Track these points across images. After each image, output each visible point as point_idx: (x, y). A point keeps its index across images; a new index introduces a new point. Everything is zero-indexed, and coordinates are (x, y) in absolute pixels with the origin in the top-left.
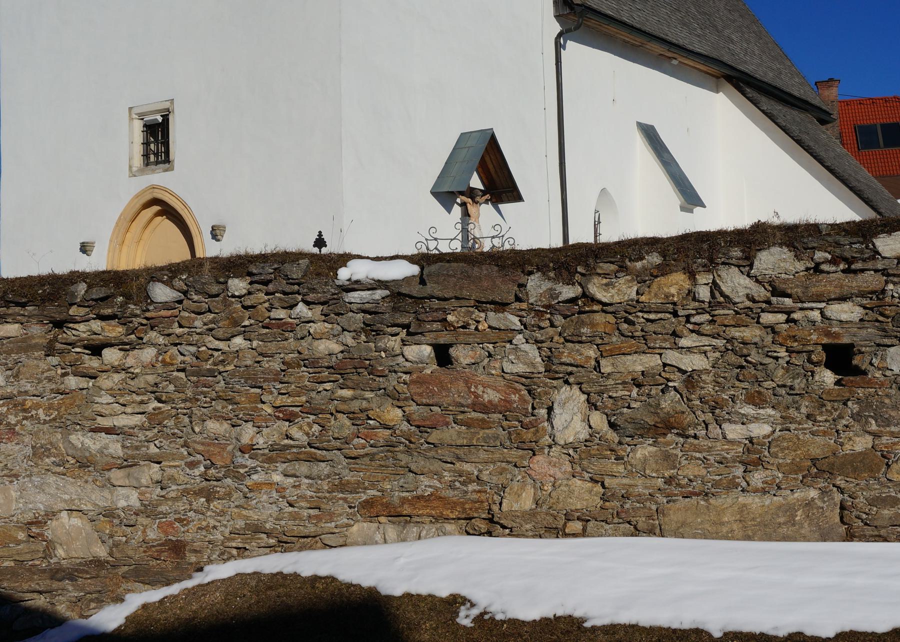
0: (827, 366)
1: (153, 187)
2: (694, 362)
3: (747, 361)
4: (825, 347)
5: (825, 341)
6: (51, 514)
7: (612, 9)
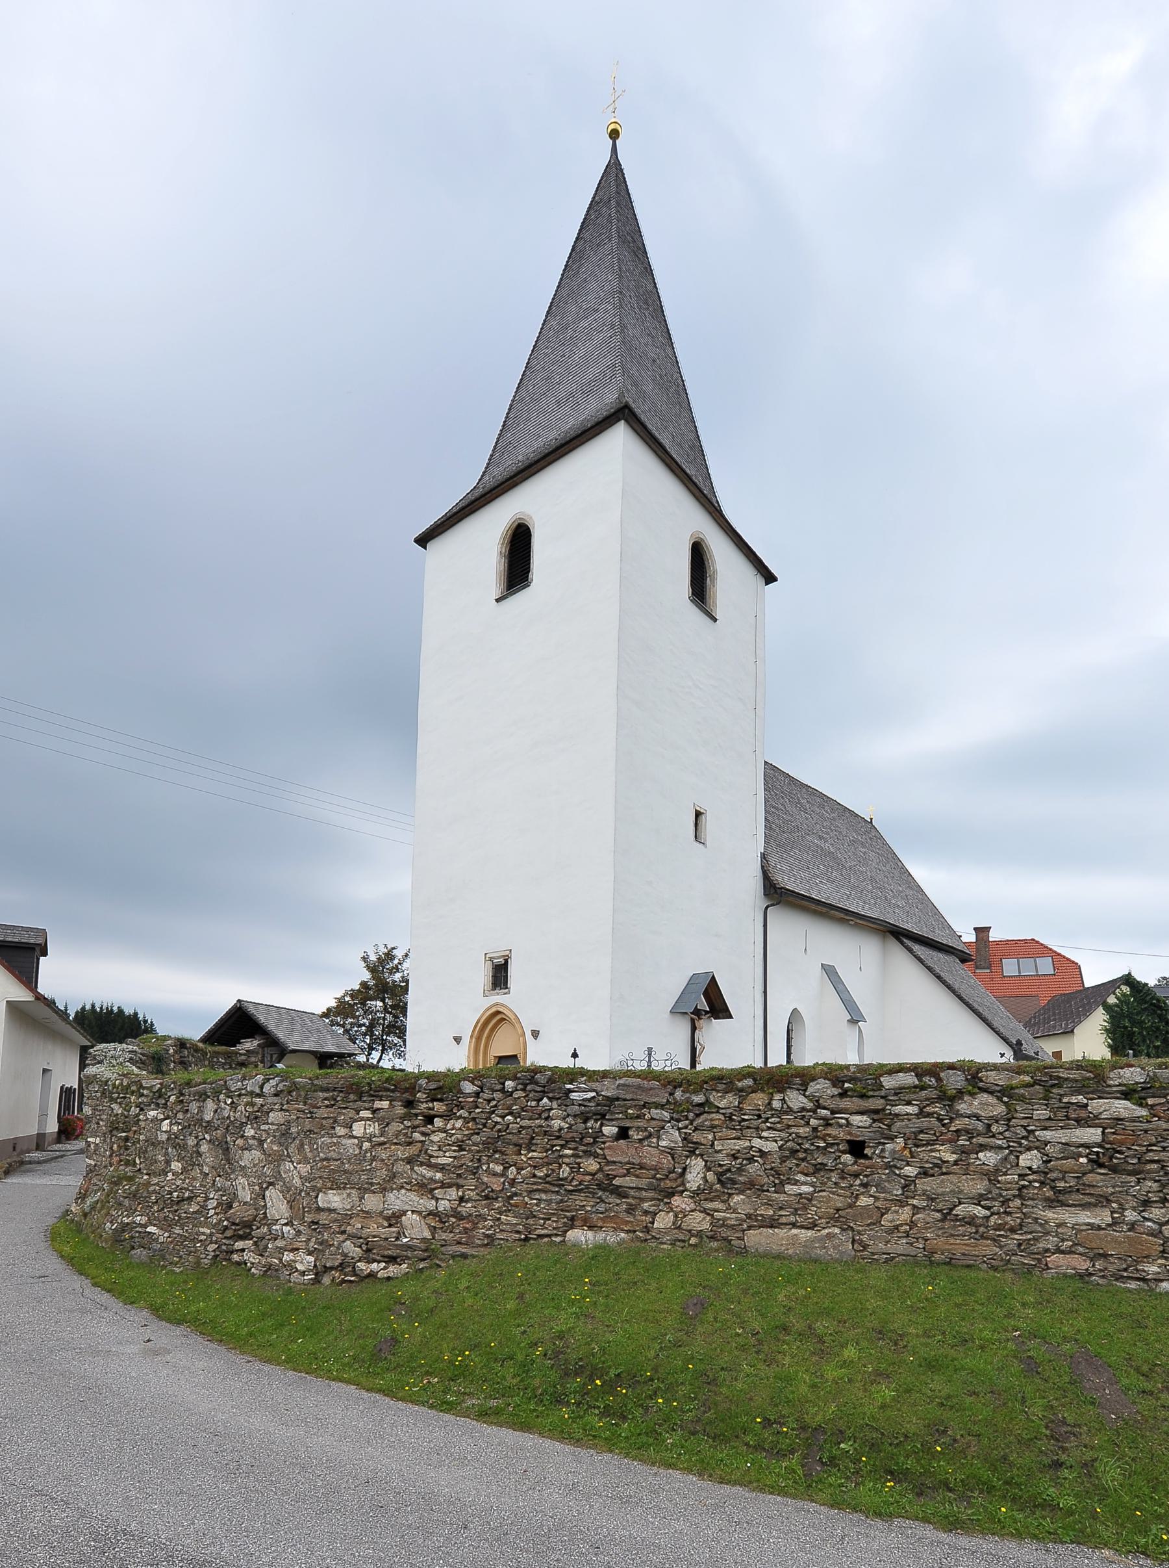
0: (850, 1153)
1: (497, 1004)
2: (769, 1146)
3: (801, 1148)
4: (848, 1142)
5: (849, 1138)
6: (404, 1213)
7: (805, 890)
